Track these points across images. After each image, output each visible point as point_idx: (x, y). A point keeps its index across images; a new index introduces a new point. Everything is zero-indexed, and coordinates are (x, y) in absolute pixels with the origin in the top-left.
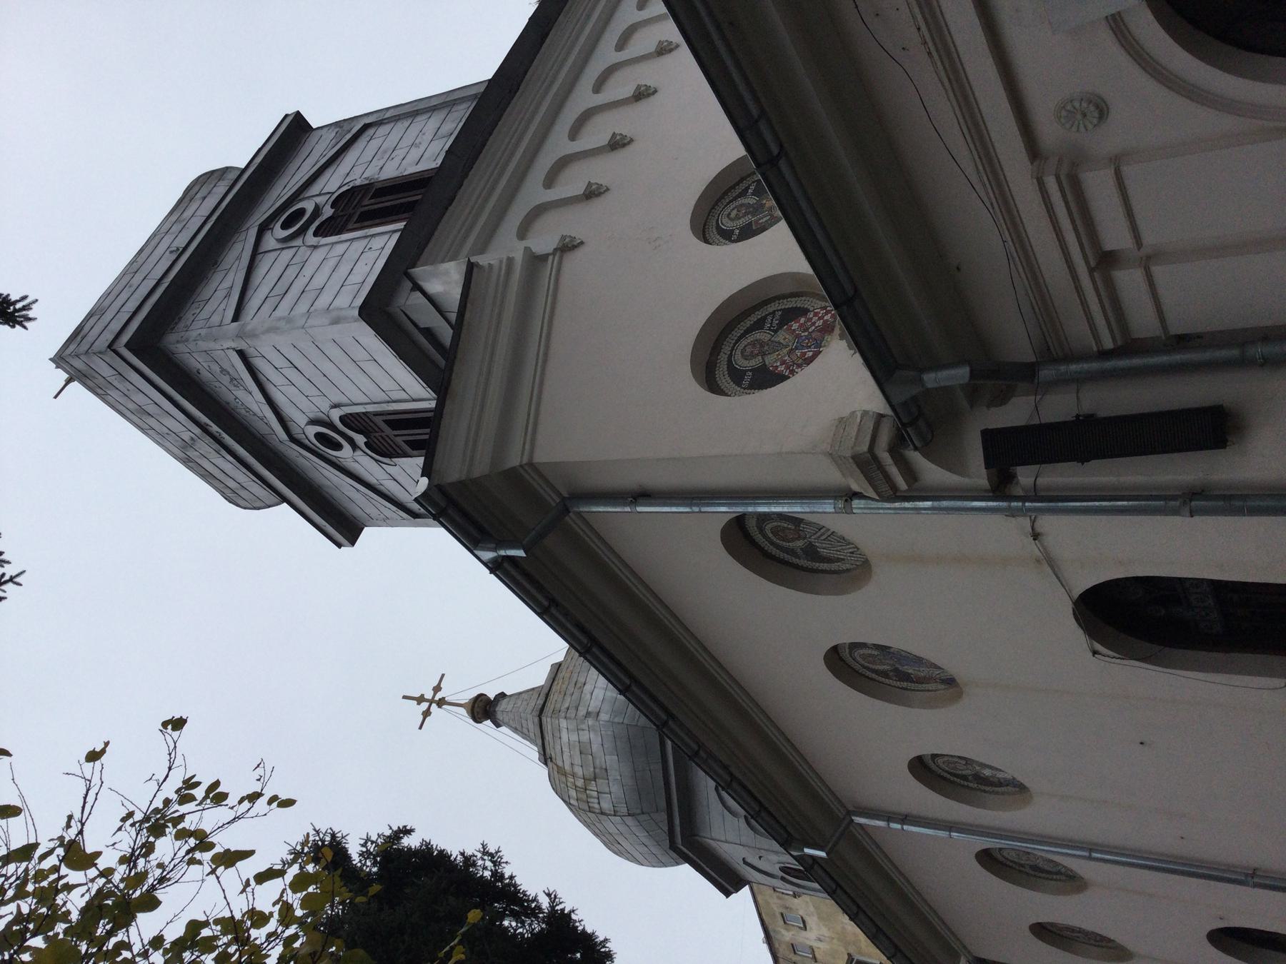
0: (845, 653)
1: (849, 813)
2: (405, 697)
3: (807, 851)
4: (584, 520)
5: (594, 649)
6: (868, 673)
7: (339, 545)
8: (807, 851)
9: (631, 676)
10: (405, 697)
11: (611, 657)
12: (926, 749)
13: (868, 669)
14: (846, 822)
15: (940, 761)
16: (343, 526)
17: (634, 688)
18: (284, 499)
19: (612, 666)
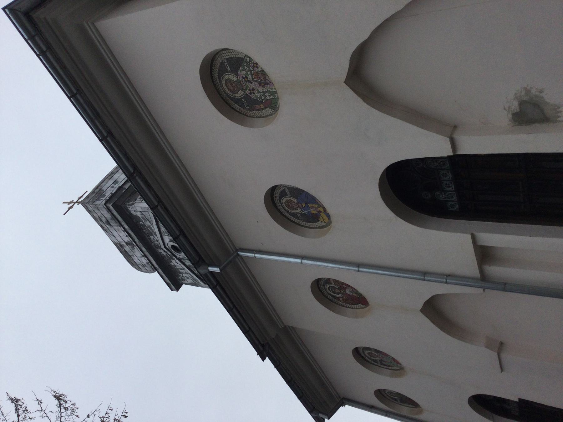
0: (361, 351)
1: (237, 250)
2: (64, 203)
3: (211, 269)
4: (243, 260)
5: (218, 287)
6: (370, 361)
7: (172, 290)
8: (211, 269)
9: (234, 306)
10: (64, 203)
11: (58, 60)
12: (362, 344)
13: (371, 359)
14: (235, 254)
15: (387, 392)
16: (175, 283)
17: (181, 237)
18: (157, 270)
19: (224, 296)
